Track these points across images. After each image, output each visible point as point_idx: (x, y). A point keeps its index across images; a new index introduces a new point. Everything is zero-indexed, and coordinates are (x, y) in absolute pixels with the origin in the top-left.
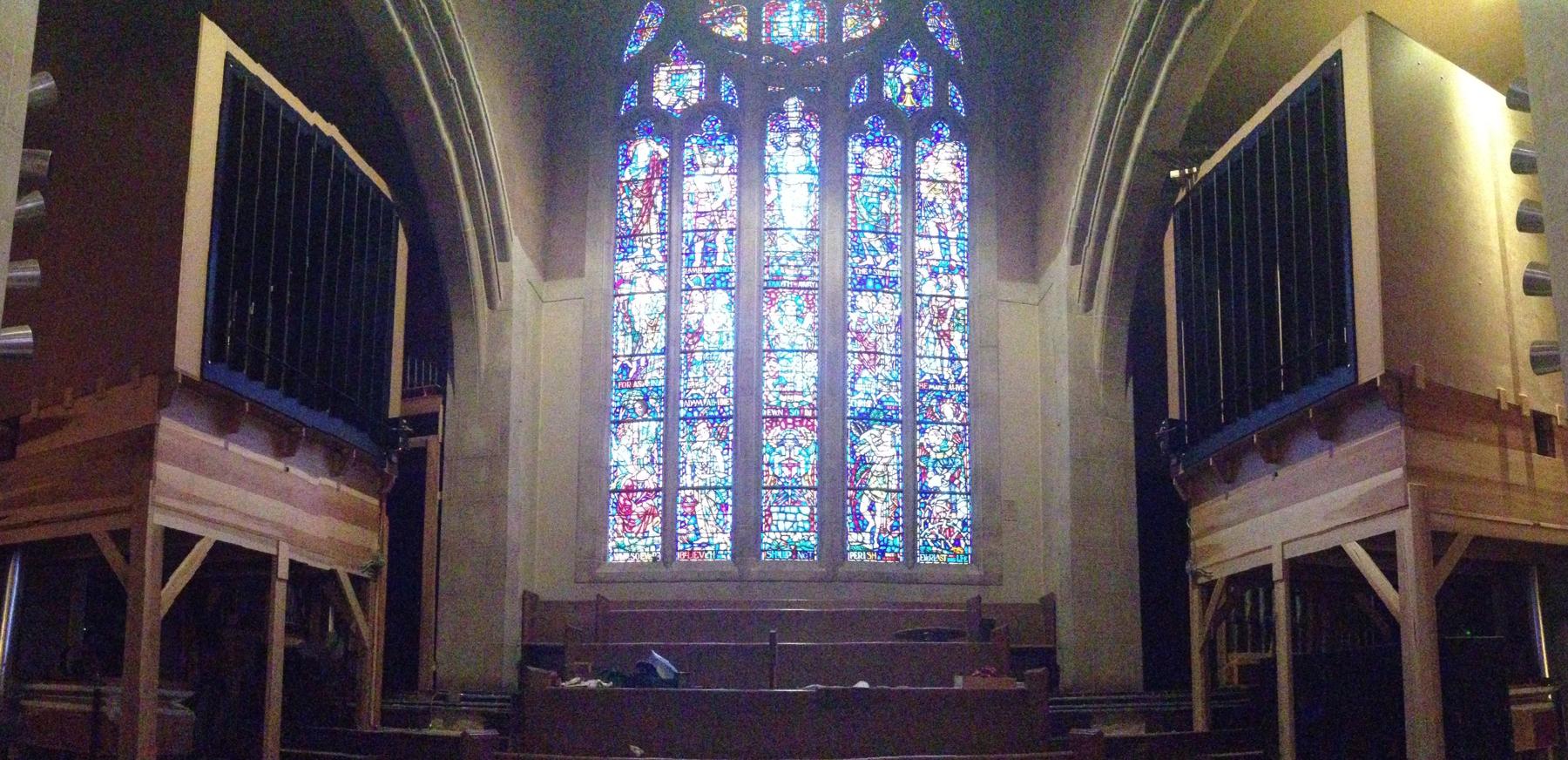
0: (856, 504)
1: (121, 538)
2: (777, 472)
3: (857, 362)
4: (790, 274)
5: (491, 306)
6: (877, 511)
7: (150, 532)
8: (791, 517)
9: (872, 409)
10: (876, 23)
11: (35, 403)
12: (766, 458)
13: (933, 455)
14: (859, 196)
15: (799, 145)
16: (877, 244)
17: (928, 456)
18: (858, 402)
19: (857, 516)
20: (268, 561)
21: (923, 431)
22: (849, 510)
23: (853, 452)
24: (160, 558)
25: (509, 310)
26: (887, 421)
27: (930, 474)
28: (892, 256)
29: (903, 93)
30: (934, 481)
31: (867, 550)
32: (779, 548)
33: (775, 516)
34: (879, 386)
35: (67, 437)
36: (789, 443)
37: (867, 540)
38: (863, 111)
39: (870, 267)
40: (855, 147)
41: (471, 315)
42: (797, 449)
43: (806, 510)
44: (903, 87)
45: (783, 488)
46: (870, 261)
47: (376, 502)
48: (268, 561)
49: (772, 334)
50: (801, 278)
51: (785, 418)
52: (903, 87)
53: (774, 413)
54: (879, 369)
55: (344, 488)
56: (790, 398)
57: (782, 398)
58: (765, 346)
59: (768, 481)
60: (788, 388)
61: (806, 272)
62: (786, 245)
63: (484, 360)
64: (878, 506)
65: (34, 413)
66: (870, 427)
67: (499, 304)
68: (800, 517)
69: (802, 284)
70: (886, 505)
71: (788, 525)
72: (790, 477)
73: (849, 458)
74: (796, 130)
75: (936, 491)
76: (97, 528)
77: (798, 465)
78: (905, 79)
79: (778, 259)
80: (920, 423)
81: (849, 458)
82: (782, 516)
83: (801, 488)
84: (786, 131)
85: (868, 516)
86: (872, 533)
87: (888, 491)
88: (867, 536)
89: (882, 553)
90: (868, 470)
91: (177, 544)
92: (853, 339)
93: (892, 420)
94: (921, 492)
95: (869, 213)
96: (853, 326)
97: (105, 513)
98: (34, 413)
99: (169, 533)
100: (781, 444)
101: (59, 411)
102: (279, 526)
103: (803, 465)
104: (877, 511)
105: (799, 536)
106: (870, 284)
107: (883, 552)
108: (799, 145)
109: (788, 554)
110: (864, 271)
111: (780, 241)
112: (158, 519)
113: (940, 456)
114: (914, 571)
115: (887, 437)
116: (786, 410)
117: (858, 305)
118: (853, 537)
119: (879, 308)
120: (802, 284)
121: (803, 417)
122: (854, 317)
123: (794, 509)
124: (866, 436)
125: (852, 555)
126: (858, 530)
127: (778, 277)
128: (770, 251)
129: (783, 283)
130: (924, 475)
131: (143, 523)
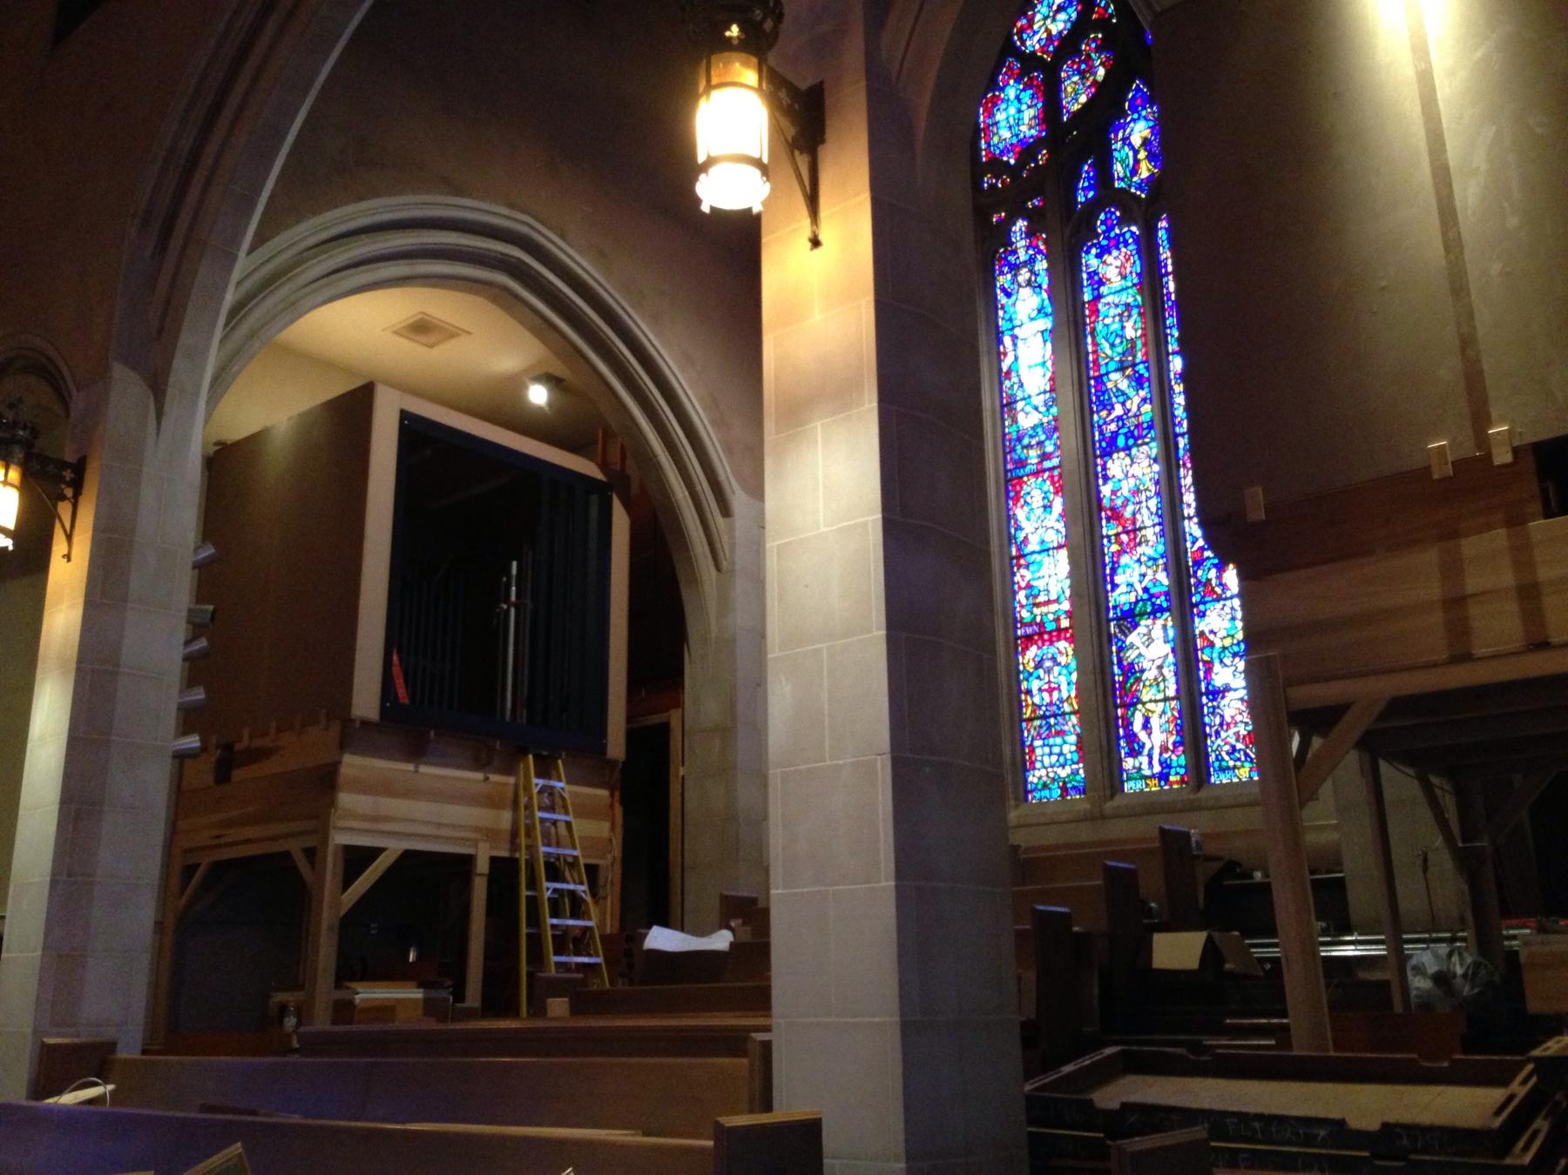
0: (1128, 724)
1: (310, 853)
2: (1037, 700)
3: (1115, 548)
4: (1033, 456)
5: (718, 568)
6: (1155, 725)
7: (331, 848)
8: (1056, 750)
9: (1137, 601)
10: (1101, 72)
11: (246, 733)
12: (1024, 686)
13: (1218, 644)
14: (1099, 327)
15: (1029, 283)
16: (1124, 385)
17: (1211, 645)
18: (1121, 598)
19: (1132, 738)
20: (467, 861)
21: (1203, 615)
22: (1121, 732)
23: (1120, 661)
24: (340, 872)
25: (732, 571)
26: (1157, 611)
27: (1217, 667)
28: (1142, 393)
29: (1137, 162)
30: (1221, 676)
31: (1146, 777)
32: (1045, 786)
33: (1038, 752)
34: (1143, 569)
35: (270, 767)
36: (1048, 664)
37: (1145, 766)
38: (1093, 207)
39: (1119, 418)
40: (1091, 260)
41: (695, 581)
42: (1056, 669)
43: (1072, 739)
44: (1136, 152)
45: (1044, 717)
46: (1118, 411)
47: (604, 793)
48: (467, 861)
49: (1021, 536)
50: (1045, 456)
51: (1041, 634)
52: (1136, 152)
53: (1029, 631)
54: (1140, 550)
55: (494, 778)
56: (1044, 609)
57: (1037, 611)
58: (1014, 552)
59: (1028, 713)
60: (1042, 598)
61: (1049, 448)
62: (1027, 419)
63: (714, 627)
64: (1155, 722)
65: (245, 742)
66: (1136, 626)
67: (725, 564)
68: (1066, 749)
69: (1047, 464)
70: (1165, 718)
71: (1054, 758)
72: (1051, 704)
73: (1116, 670)
74: (1025, 264)
75: (1227, 689)
76: (295, 847)
77: (1058, 688)
78: (1136, 140)
79: (1019, 439)
80: (1197, 605)
81: (1116, 670)
82: (1047, 750)
83: (1063, 714)
84: (1015, 268)
85: (1143, 736)
86: (1150, 757)
87: (1166, 699)
88: (1144, 760)
89: (1163, 776)
90: (1138, 680)
91: (356, 859)
92: (1108, 519)
93: (1161, 610)
94: (1208, 693)
95: (1112, 345)
96: (1106, 502)
97: (301, 834)
98: (245, 742)
99: (349, 850)
100: (1039, 665)
101: (267, 742)
102: (477, 829)
103: (1064, 687)
104: (1155, 725)
105: (1068, 770)
106: (1121, 441)
107: (1168, 774)
108: (1029, 283)
109: (1057, 793)
110: (1113, 427)
111: (1021, 416)
112: (340, 839)
113: (1227, 642)
114: (1202, 794)
115: (1157, 632)
116: (1042, 625)
117: (1110, 474)
118: (1129, 763)
119: (1136, 470)
120: (1047, 464)
121: (1059, 630)
122: (1106, 490)
123: (1058, 740)
124: (1133, 638)
125: (1129, 787)
126: (1133, 753)
127: (1022, 463)
128: (1011, 430)
129: (1028, 469)
130: (1209, 671)
131: (325, 840)
